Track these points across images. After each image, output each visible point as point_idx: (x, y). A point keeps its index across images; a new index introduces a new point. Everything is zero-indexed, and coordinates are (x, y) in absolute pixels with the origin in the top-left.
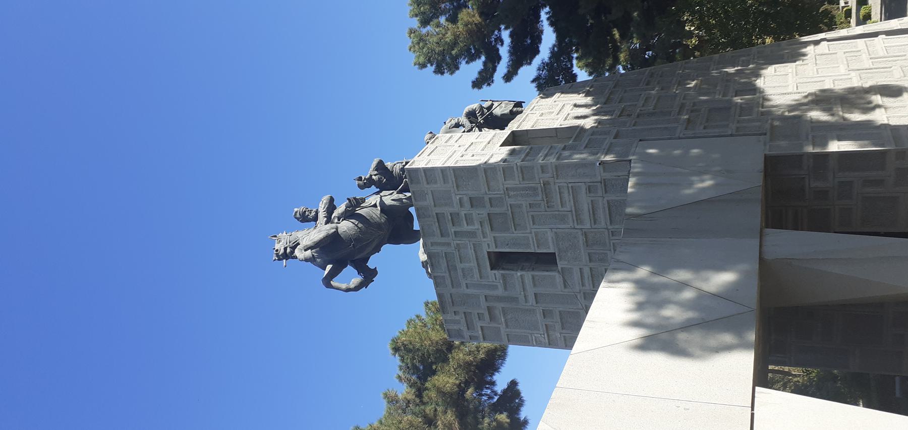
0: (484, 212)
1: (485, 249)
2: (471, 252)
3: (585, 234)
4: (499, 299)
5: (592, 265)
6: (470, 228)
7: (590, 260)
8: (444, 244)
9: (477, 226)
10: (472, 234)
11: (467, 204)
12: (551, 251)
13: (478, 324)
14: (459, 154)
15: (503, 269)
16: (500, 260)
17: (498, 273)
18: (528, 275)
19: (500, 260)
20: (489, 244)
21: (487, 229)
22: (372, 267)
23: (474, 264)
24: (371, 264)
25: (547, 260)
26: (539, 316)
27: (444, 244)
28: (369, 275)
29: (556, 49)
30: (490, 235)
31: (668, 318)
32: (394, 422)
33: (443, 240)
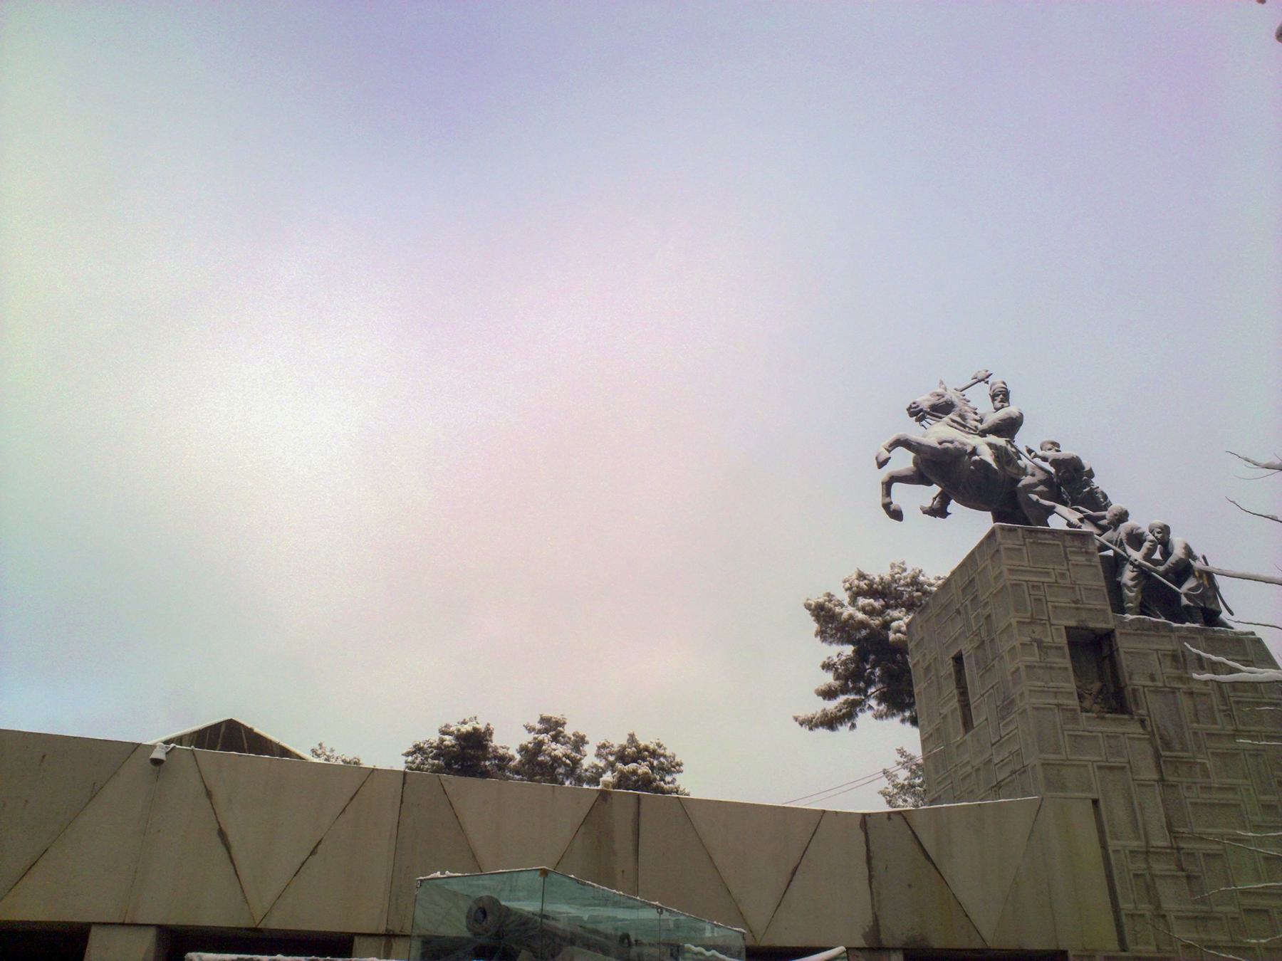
16: (958, 659)
18: (955, 703)
19: (958, 659)
22: (949, 509)
24: (954, 506)
25: (967, 724)
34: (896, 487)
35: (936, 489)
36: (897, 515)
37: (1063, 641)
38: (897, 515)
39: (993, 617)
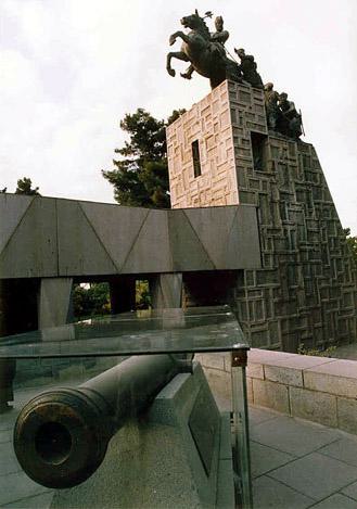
10: (203, 128)
19: (195, 144)
25: (198, 173)
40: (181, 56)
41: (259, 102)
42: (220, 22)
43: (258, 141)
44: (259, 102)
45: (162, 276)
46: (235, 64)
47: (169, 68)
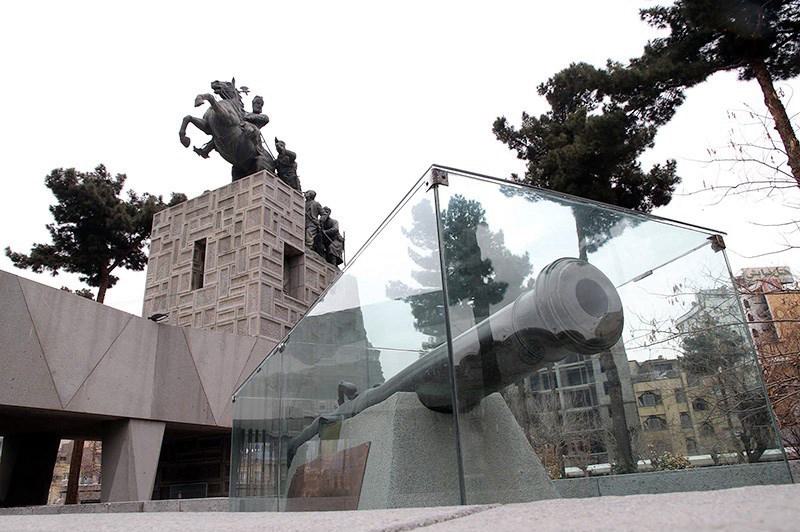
0: (232, 233)
1: (208, 236)
2: (206, 225)
3: (213, 309)
4: (176, 250)
5: (194, 315)
6: (223, 224)
7: (197, 314)
8: (214, 204)
9: (223, 228)
10: (218, 226)
11: (238, 219)
12: (204, 285)
13: (162, 236)
14: (278, 210)
15: (195, 251)
16: (201, 245)
17: (192, 248)
18: (190, 269)
19: (201, 245)
20: (210, 237)
21: (222, 236)
23: (200, 228)
24: (213, 154)
25: (198, 282)
26: (164, 280)
27: (214, 204)
28: (204, 153)
29: (435, 332)
30: (216, 239)
31: (237, 476)
32: (508, 473)
33: (216, 203)
34: (190, 125)
35: (210, 138)
36: (186, 142)
37: (282, 250)
38: (186, 142)
39: (244, 222)
40: (204, 126)
41: (299, 210)
42: (258, 103)
43: (291, 257)
44: (299, 210)
45: (132, 425)
46: (269, 156)
47: (182, 134)
